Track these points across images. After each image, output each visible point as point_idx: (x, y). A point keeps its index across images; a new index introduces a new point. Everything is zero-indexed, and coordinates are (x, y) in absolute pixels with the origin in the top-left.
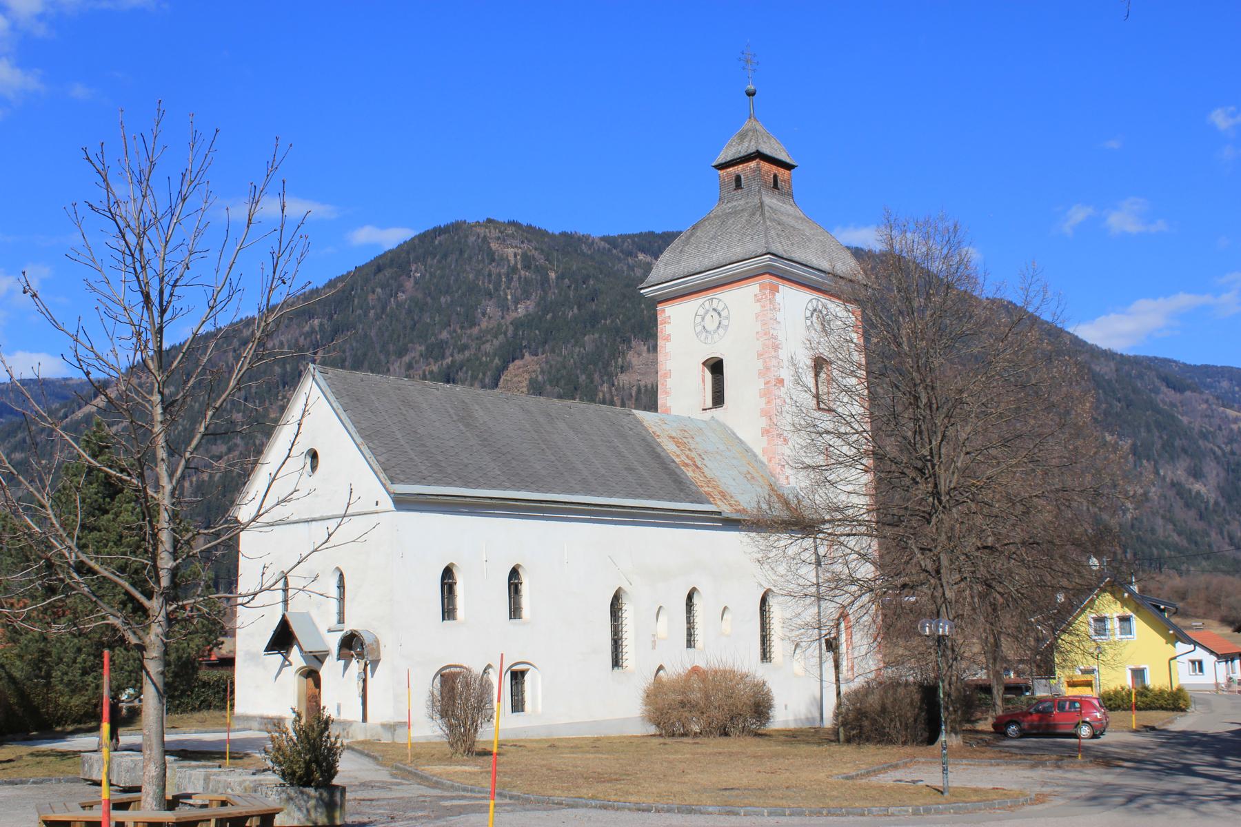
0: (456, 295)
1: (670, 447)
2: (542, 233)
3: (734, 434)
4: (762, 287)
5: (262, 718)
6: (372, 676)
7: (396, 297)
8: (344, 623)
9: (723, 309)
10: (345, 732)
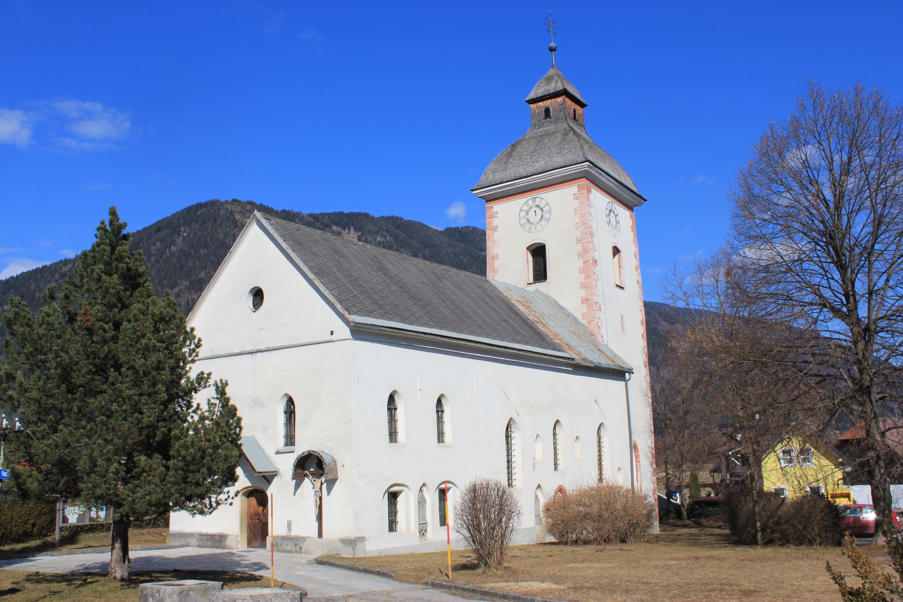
0: (211, 249)
1: (522, 308)
3: (556, 303)
4: (580, 188)
5: (201, 535)
6: (329, 493)
7: (170, 248)
9: (545, 206)
10: (298, 547)
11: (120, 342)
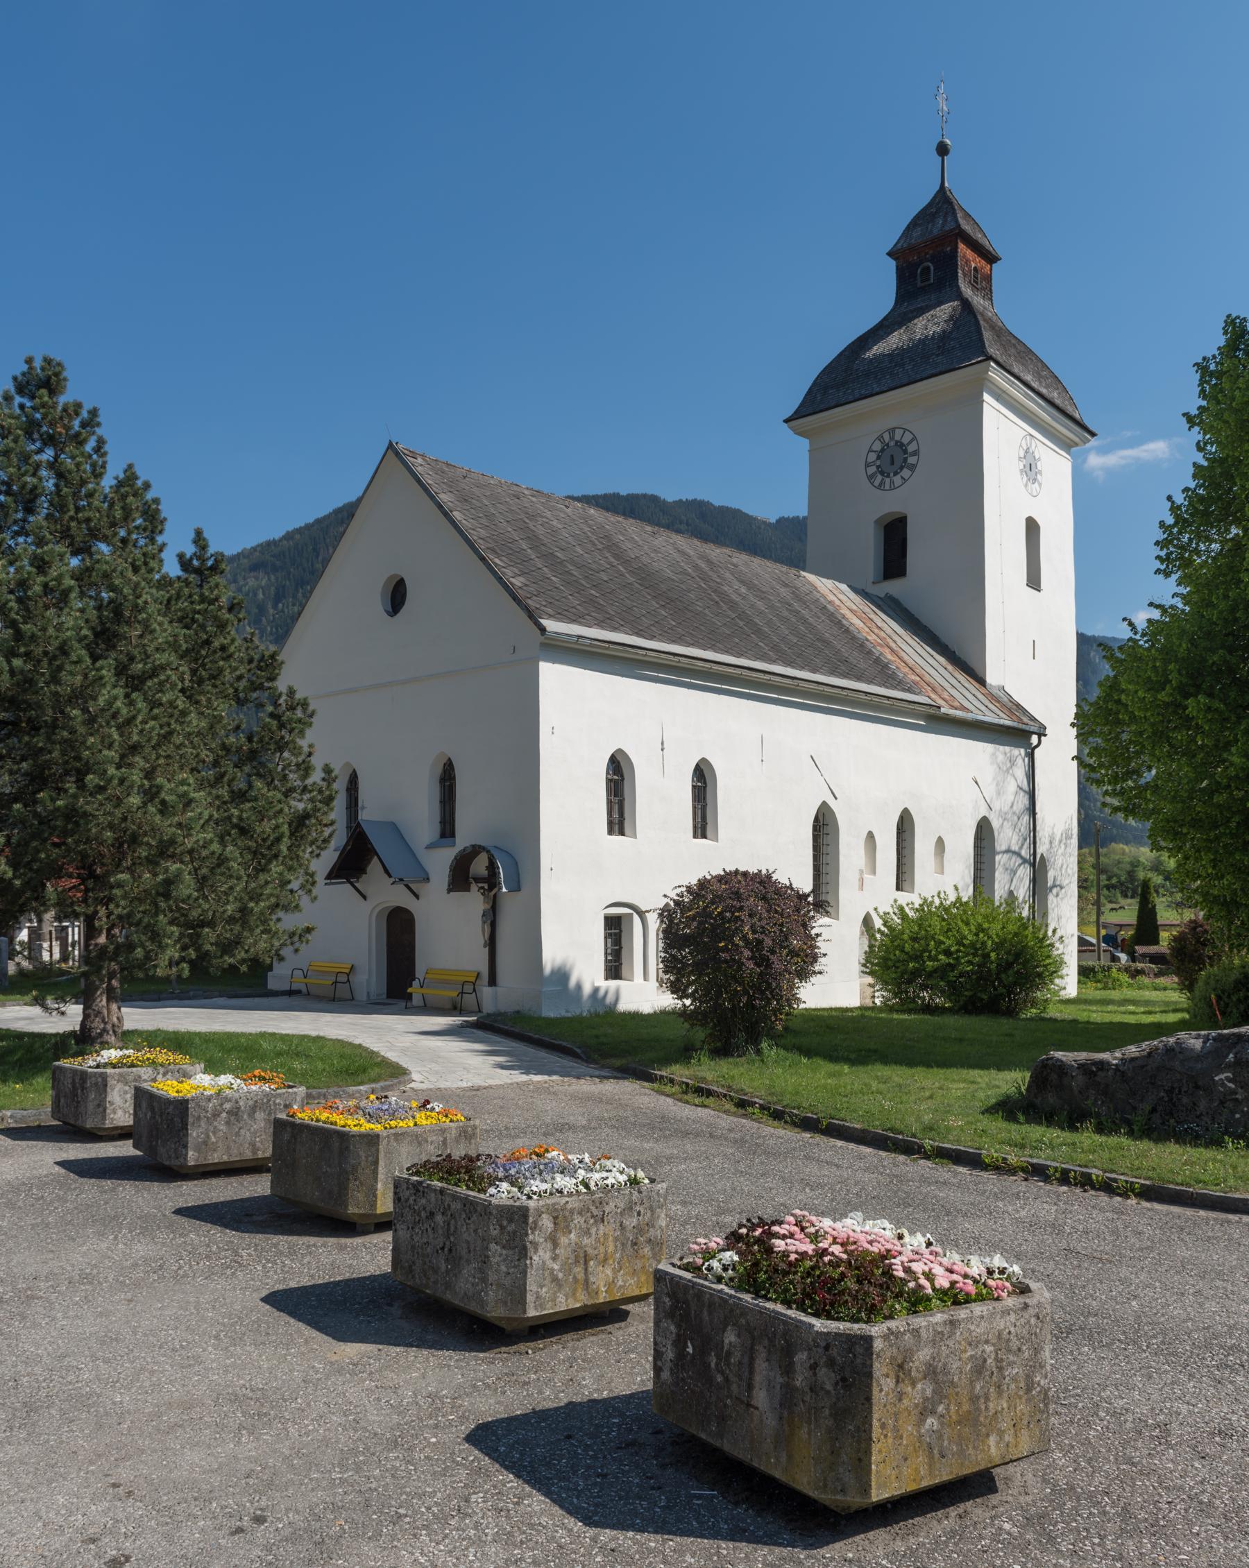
8: (453, 835)
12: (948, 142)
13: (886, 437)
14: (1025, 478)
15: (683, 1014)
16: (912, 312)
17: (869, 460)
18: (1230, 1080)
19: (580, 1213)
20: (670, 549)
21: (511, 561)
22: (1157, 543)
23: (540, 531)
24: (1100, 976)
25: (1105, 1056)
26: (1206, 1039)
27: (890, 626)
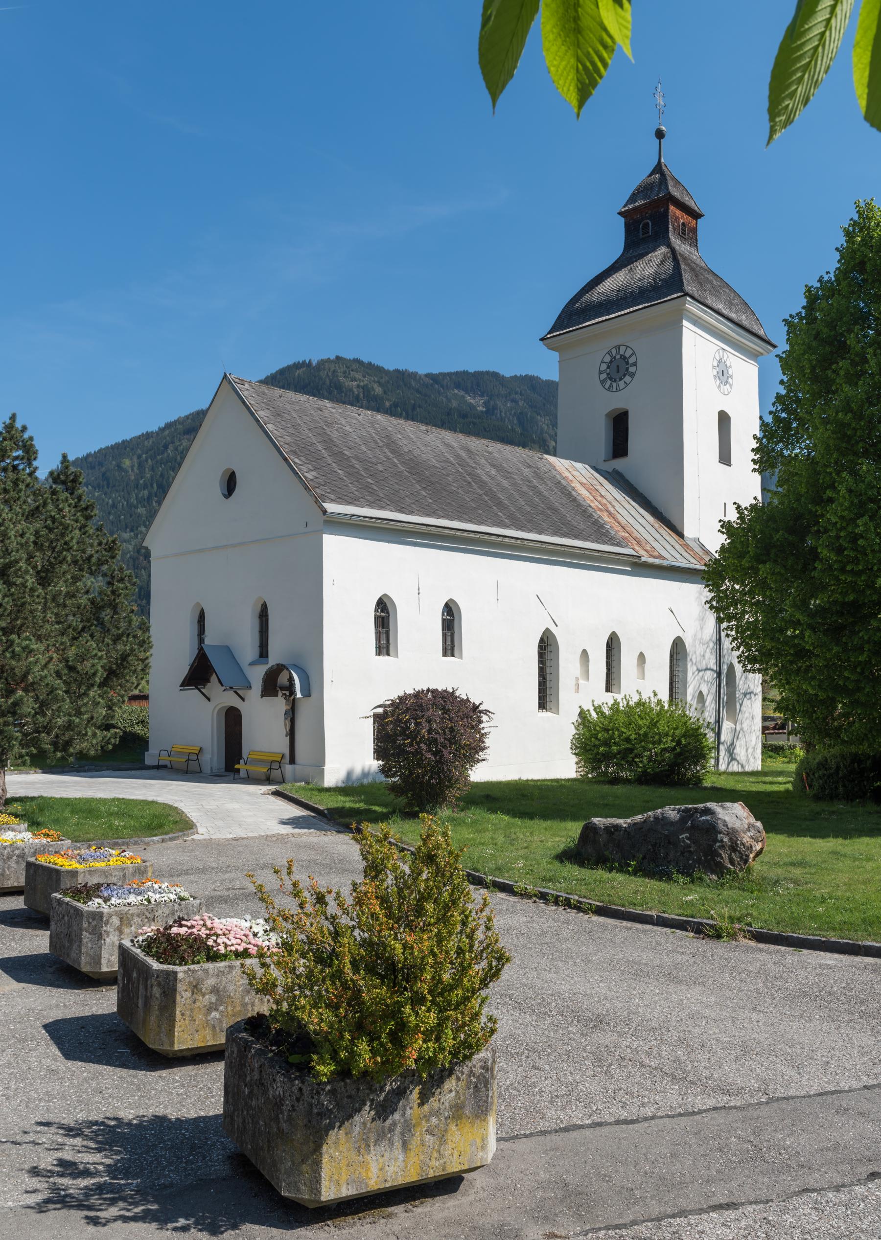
2: (379, 370)
8: (267, 656)
11: (484, 914)
12: (663, 128)
13: (614, 352)
14: (718, 381)
15: (393, 788)
16: (635, 257)
17: (602, 369)
18: (688, 838)
19: (138, 916)
20: (438, 443)
21: (307, 459)
22: (753, 450)
23: (335, 435)
24: (787, 753)
25: (620, 822)
26: (679, 811)
27: (611, 493)
